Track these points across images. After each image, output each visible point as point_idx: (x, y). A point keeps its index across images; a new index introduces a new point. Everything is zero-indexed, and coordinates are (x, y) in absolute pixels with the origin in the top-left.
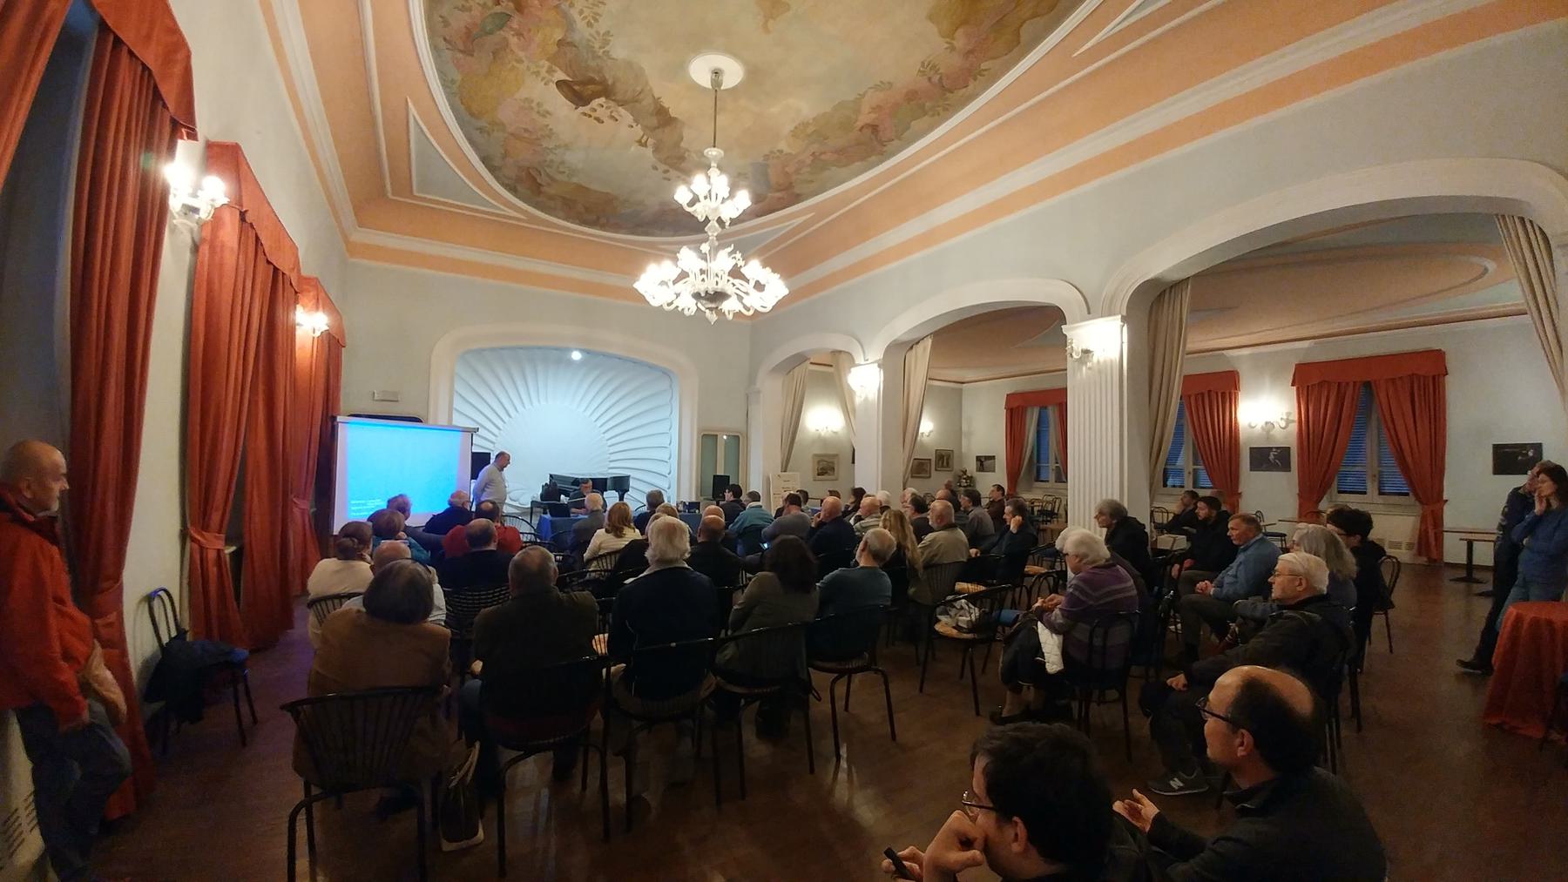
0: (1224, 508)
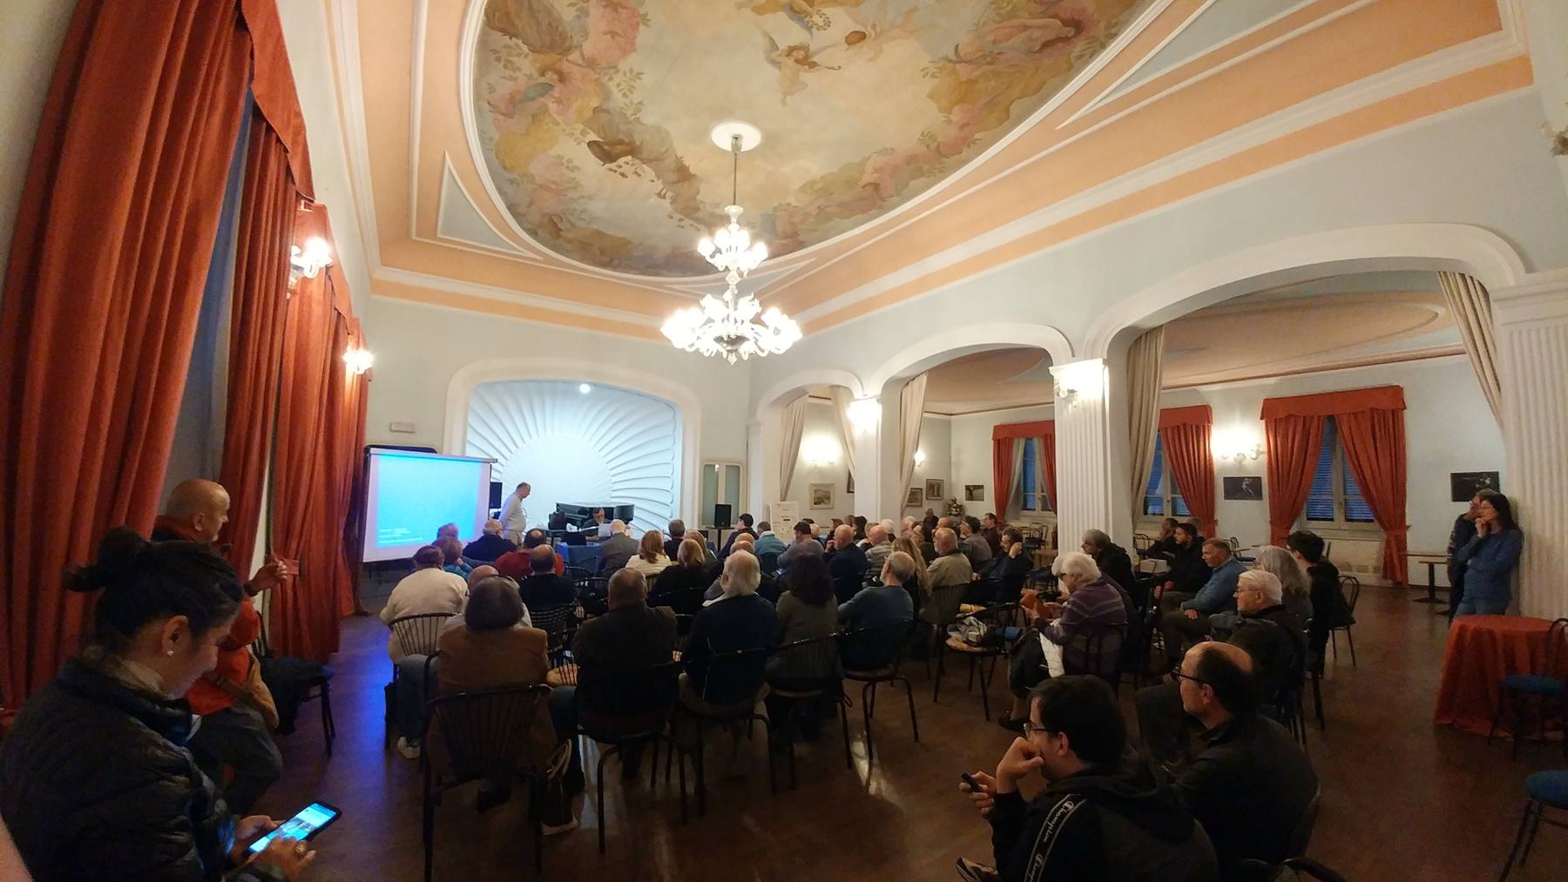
0: (1200, 534)
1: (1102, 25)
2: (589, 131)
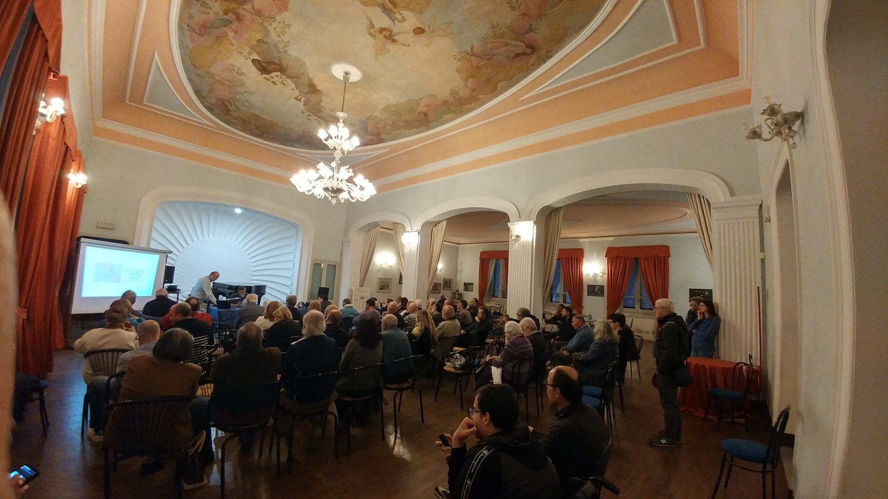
0: (574, 312)
1: (544, 51)
2: (253, 52)
